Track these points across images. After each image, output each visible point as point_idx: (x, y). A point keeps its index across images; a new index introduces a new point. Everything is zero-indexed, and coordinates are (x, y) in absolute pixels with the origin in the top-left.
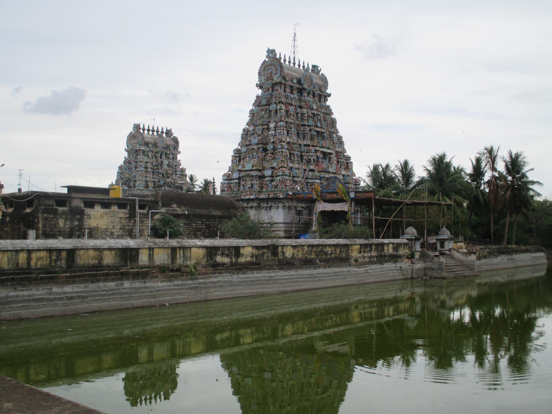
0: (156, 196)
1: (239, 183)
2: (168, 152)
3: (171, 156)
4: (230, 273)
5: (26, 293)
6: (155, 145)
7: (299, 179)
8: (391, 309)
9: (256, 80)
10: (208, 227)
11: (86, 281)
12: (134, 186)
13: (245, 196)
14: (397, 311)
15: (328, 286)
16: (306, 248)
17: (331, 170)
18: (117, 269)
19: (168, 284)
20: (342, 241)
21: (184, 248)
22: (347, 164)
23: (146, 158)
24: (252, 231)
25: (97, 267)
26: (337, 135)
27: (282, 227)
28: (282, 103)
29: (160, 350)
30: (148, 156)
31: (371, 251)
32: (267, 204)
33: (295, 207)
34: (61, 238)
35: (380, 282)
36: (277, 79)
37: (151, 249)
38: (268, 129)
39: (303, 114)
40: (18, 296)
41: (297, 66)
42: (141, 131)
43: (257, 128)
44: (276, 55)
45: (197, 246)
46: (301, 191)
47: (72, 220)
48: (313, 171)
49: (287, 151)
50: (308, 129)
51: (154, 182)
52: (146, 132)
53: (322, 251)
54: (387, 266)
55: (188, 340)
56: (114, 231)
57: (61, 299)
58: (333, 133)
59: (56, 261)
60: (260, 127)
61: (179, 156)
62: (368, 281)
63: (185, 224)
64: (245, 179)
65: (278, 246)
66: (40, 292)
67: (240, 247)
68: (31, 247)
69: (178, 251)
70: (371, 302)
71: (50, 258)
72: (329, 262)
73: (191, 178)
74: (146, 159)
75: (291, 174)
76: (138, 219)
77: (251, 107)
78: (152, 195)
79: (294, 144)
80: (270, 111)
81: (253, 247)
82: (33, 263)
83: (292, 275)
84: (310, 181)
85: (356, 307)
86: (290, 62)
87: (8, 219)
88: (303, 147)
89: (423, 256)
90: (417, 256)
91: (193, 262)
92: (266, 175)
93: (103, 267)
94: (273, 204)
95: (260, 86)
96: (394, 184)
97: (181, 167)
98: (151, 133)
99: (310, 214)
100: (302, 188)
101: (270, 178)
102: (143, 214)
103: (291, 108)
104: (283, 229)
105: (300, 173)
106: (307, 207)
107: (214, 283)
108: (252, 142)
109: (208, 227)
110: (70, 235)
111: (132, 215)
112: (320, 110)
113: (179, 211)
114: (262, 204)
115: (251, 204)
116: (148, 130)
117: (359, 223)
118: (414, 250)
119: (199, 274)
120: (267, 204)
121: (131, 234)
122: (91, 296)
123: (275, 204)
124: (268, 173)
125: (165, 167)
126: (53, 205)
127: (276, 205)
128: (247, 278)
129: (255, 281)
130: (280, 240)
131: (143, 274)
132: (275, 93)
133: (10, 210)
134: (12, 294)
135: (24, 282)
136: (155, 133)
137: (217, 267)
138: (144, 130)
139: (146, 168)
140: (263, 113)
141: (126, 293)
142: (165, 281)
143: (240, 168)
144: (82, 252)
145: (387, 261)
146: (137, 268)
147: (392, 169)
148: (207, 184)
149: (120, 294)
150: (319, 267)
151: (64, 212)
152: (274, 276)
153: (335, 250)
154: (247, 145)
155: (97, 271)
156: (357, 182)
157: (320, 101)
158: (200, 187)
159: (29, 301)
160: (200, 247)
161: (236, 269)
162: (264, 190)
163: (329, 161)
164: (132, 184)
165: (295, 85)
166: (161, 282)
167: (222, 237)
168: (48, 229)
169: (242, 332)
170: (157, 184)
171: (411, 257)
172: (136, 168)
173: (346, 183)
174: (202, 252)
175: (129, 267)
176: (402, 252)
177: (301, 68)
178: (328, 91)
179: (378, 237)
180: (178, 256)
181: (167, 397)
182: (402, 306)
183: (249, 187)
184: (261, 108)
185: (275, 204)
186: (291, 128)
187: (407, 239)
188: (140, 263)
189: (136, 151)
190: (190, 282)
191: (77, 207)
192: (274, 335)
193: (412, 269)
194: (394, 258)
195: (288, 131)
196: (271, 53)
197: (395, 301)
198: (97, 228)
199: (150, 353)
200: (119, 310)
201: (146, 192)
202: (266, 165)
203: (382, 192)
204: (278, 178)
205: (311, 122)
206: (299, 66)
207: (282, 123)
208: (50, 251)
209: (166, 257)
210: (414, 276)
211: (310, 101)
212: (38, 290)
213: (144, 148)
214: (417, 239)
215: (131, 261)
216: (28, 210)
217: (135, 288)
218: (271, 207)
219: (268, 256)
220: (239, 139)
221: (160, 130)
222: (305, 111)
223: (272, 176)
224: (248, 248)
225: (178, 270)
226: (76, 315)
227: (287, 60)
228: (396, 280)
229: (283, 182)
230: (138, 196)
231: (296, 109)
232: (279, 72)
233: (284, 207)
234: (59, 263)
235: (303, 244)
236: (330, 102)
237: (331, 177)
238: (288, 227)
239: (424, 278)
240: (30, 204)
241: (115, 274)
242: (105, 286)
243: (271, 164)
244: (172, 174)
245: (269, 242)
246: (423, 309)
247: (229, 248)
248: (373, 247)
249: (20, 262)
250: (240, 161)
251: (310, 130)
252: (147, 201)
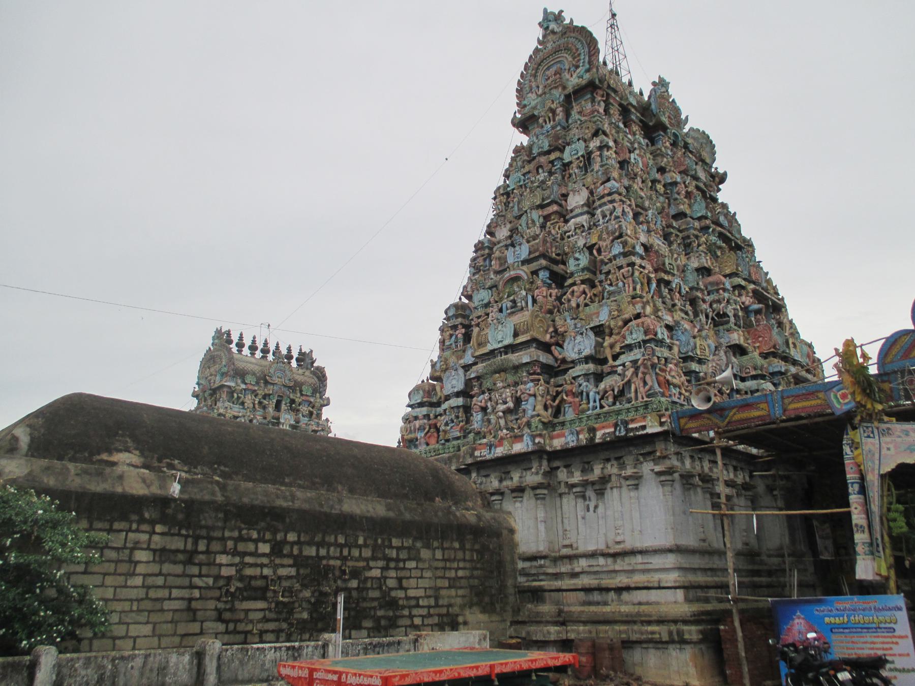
9: (510, 107)
10: (315, 573)
13: (491, 446)
30: (243, 404)
38: (564, 216)
52: (246, 351)
63: (162, 555)
64: (487, 384)
94: (612, 469)
98: (258, 354)
104: (671, 578)
108: (510, 260)
109: (315, 573)
114: (562, 475)
115: (516, 476)
123: (622, 466)
124: (579, 346)
127: (629, 471)
138: (240, 345)
144: (547, 594)
183: (507, 412)
185: (622, 466)
213: (232, 384)
218: (604, 480)
238: (694, 570)
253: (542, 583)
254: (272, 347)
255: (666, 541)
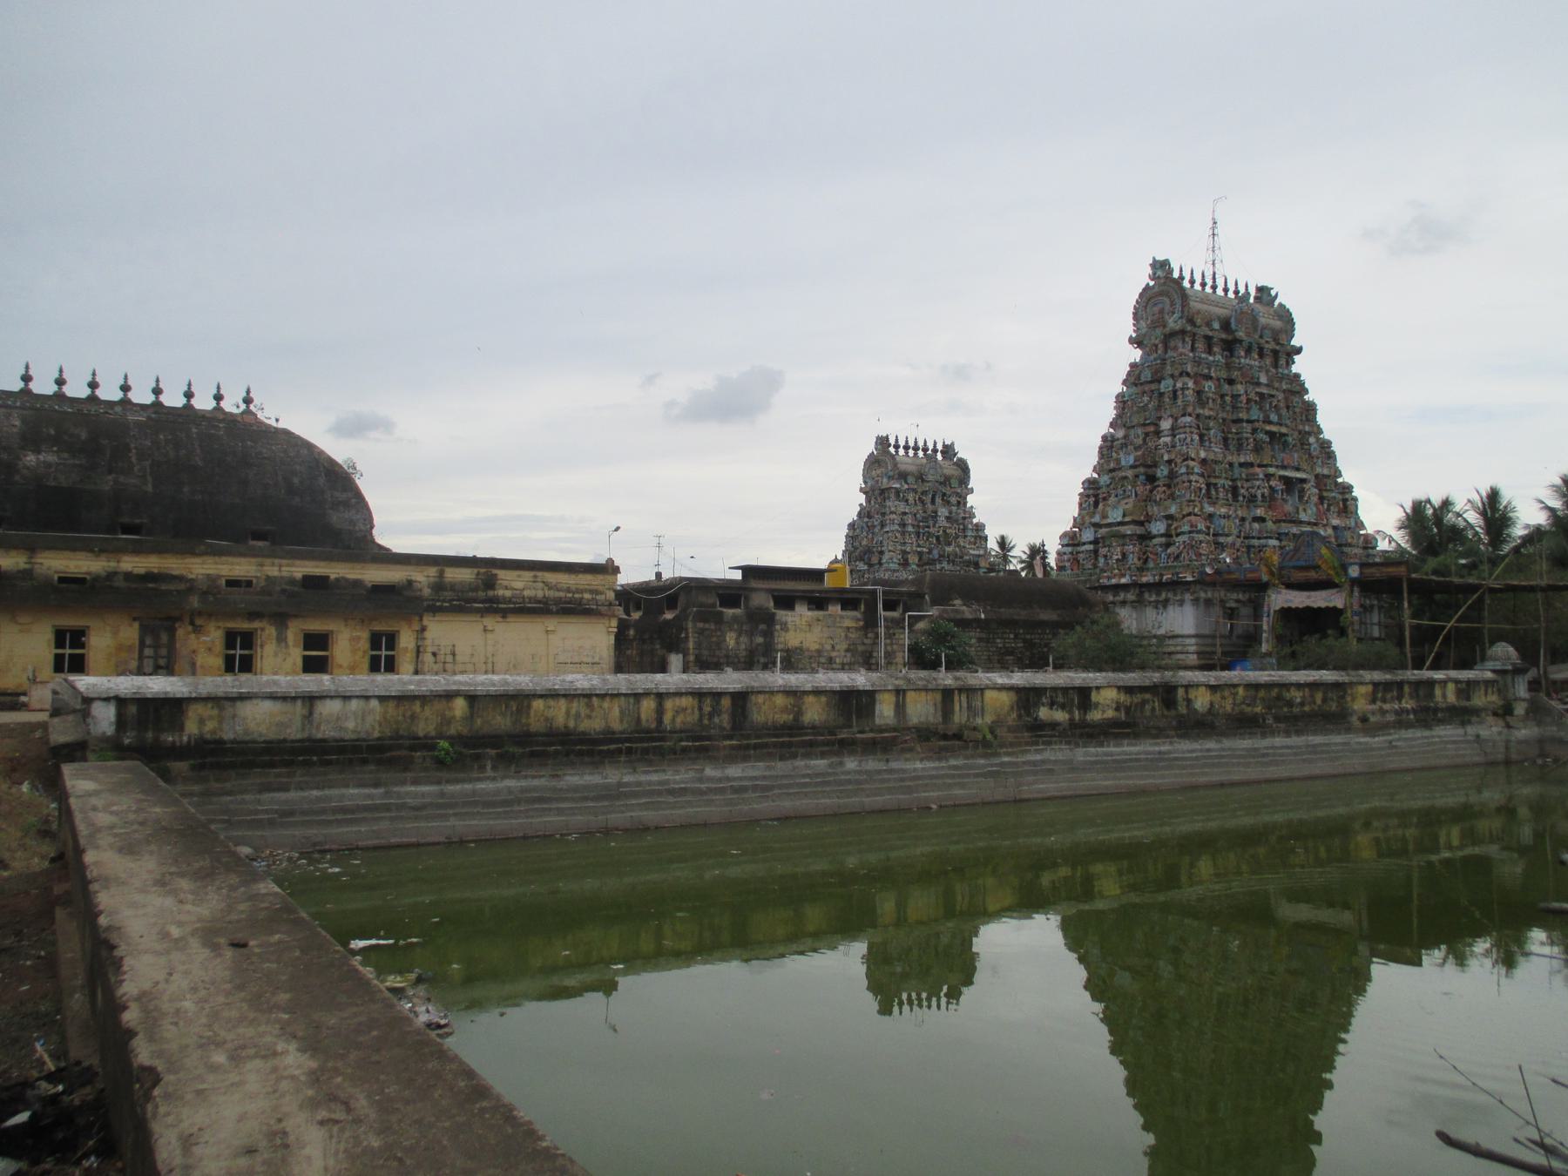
0: (918, 582)
1: (1096, 552)
2: (948, 491)
3: (953, 500)
4: (1068, 743)
5: (655, 777)
6: (921, 477)
7: (1230, 539)
8: (1455, 832)
9: (1129, 329)
10: (1030, 645)
11: (770, 756)
12: (880, 564)
13: (1109, 578)
14: (1470, 837)
15: (1297, 774)
16: (1241, 691)
17: (1303, 517)
18: (832, 733)
19: (937, 764)
20: (1327, 676)
21: (969, 691)
22: (1344, 501)
23: (902, 504)
24: (1119, 655)
25: (790, 728)
26: (1318, 439)
27: (1192, 645)
28: (1188, 375)
29: (922, 902)
31: (1400, 698)
32: (1158, 594)
33: (1222, 601)
34: (729, 670)
35: (1422, 769)
36: (1174, 323)
37: (899, 693)
38: (1158, 433)
39: (1235, 397)
40: (639, 784)
41: (1220, 292)
42: (892, 450)
43: (1132, 432)
44: (1171, 271)
45: (998, 685)
46: (1233, 567)
47: (751, 634)
48: (1261, 520)
49: (1201, 480)
50: (1248, 428)
51: (920, 554)
52: (901, 452)
53: (1279, 698)
54: (1442, 733)
55: (980, 882)
56: (834, 654)
57: (722, 791)
58: (1309, 434)
59: (711, 716)
60: (1140, 431)
61: (969, 498)
62: (1392, 766)
63: (980, 640)
65: (1174, 688)
66: (679, 775)
67: (1090, 689)
68: (662, 689)
69: (956, 698)
70: (1404, 816)
71: (700, 709)
72: (1296, 721)
73: (1003, 543)
74: (902, 507)
75: (1209, 530)
76: (882, 631)
77: (1119, 388)
78: (913, 582)
79: (1216, 462)
80: (1161, 395)
81: (1119, 688)
82: (667, 718)
83: (1208, 750)
84: (1256, 542)
85: (1367, 825)
86: (1203, 285)
87: (632, 632)
88: (1237, 470)
89: (1536, 712)
90: (1520, 709)
91: (989, 719)
92: (1155, 532)
93: (803, 728)
94: (1170, 595)
95: (1137, 342)
96: (1462, 544)
97: (975, 521)
98: (911, 453)
99: (1257, 615)
100: (1236, 560)
101: (1163, 540)
102: (893, 620)
103: (1209, 386)
104: (1193, 649)
105: (1232, 526)
106: (1250, 600)
107: (1034, 763)
109: (1030, 645)
110: (748, 664)
111: (870, 622)
112: (1276, 385)
113: (967, 613)
114: (1146, 595)
116: (906, 448)
117: (1376, 633)
118: (1510, 696)
119: (1001, 746)
120: (1158, 594)
121: (868, 662)
122: (780, 787)
124: (1158, 527)
125: (942, 521)
126: (714, 605)
128: (1106, 754)
129: (1125, 761)
130: (1181, 673)
131: (884, 744)
132: (1170, 353)
133: (636, 615)
134: (626, 779)
135: (651, 756)
136: (921, 454)
137: (1040, 732)
138: (897, 447)
139: (903, 525)
140: (1146, 399)
141: (849, 782)
142: (929, 759)
143: (1097, 519)
144: (760, 699)
145: (1441, 722)
146: (872, 731)
147: (1457, 508)
148: (1037, 552)
149: (840, 783)
150: (1273, 733)
151: (735, 618)
152: (1169, 752)
153: (1312, 696)
154: (1111, 471)
155: (791, 736)
156: (1369, 542)
157: (1276, 366)
158: (1022, 562)
159: (660, 793)
160: (1002, 688)
161: (1081, 736)
162: (1151, 565)
163: (1301, 498)
164: (875, 560)
165: (1216, 334)
166: (922, 760)
167: (1058, 667)
168: (706, 653)
169: (1098, 868)
170: (925, 557)
171: (1505, 711)
172: (883, 525)
173: (1339, 545)
174: (1006, 699)
175: (855, 729)
176: (1479, 700)
177: (1231, 295)
178: (1295, 342)
179: (1418, 665)
180: (957, 708)
181: (954, 995)
182: (1483, 825)
184: (1140, 388)
186: (1208, 429)
187: (1494, 671)
188: (878, 721)
189: (883, 491)
190: (982, 761)
191: (760, 608)
192: (1171, 879)
193: (1508, 742)
194: (1462, 714)
195: (1201, 436)
196: (1161, 268)
197: (1463, 814)
198: (800, 650)
199: (901, 905)
200: (836, 816)
201: (903, 575)
202: (1154, 510)
203: (1432, 563)
204: (1181, 539)
205: (1255, 414)
206: (1226, 290)
207: (1188, 419)
208: (699, 695)
209: (932, 710)
210: (1514, 757)
211: (1251, 367)
212: (677, 772)
214: (1517, 671)
215: (859, 717)
216: (669, 616)
217: (867, 772)
219: (1153, 709)
220: (1094, 459)
221: (931, 447)
222: (1240, 389)
223: (1168, 535)
224: (1107, 690)
225: (958, 736)
226: (753, 823)
227: (1198, 280)
228: (1466, 766)
229: (1191, 546)
230: (883, 583)
231: (1219, 386)
232: (1178, 307)
233: (1196, 601)
234: (716, 720)
235: (1235, 681)
236: (1299, 365)
237: (1303, 533)
239: (1540, 762)
240: (672, 602)
241: (827, 743)
242: (807, 767)
243: (1166, 508)
244: (957, 537)
245: (1155, 677)
246: (1538, 835)
247: (1065, 690)
248: (1406, 689)
249: (643, 717)
250: (1096, 504)
251: (1254, 431)
252: (898, 593)
253: (334, 830)
254: (921, 444)
255: (1192, 631)
